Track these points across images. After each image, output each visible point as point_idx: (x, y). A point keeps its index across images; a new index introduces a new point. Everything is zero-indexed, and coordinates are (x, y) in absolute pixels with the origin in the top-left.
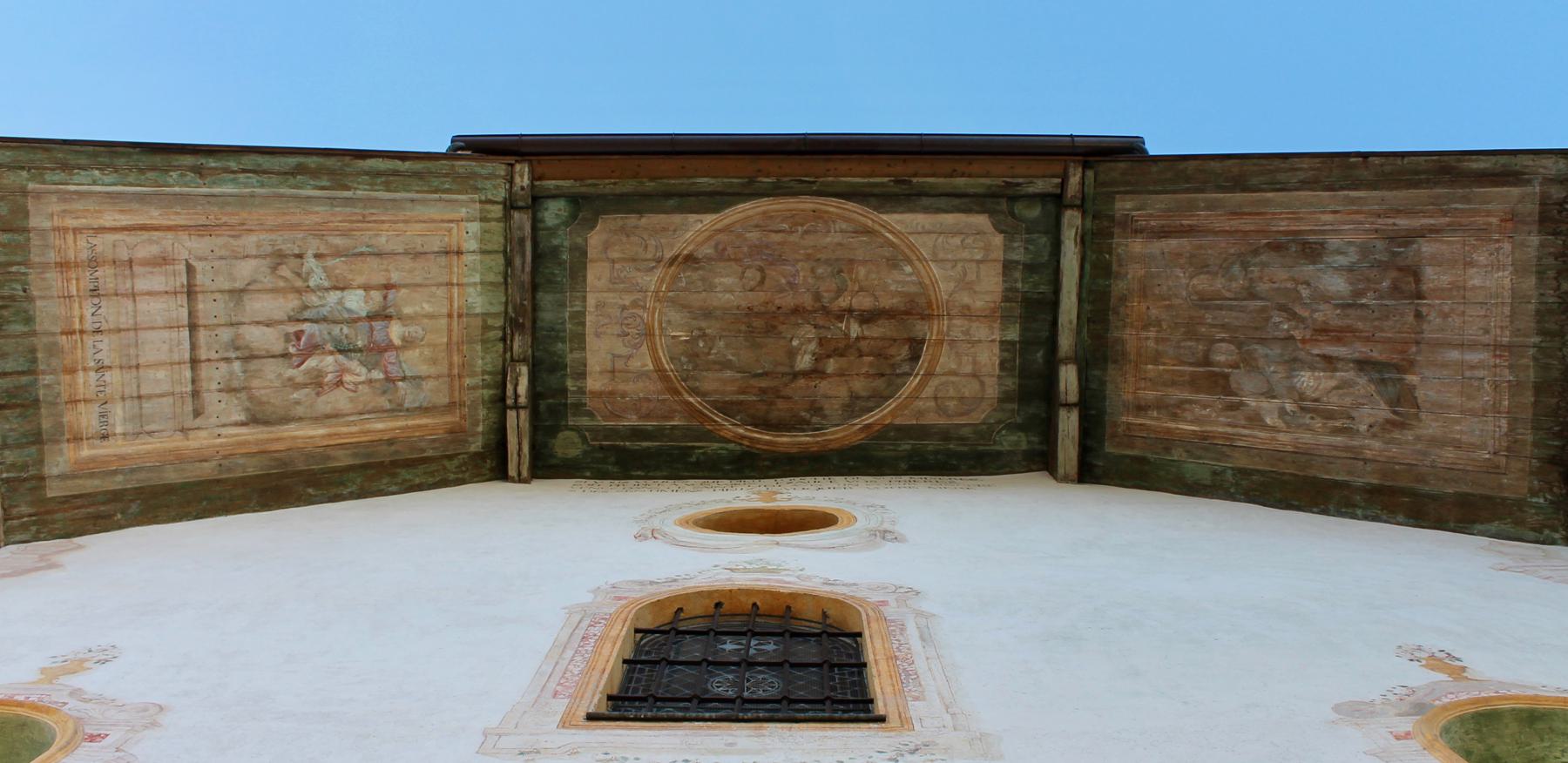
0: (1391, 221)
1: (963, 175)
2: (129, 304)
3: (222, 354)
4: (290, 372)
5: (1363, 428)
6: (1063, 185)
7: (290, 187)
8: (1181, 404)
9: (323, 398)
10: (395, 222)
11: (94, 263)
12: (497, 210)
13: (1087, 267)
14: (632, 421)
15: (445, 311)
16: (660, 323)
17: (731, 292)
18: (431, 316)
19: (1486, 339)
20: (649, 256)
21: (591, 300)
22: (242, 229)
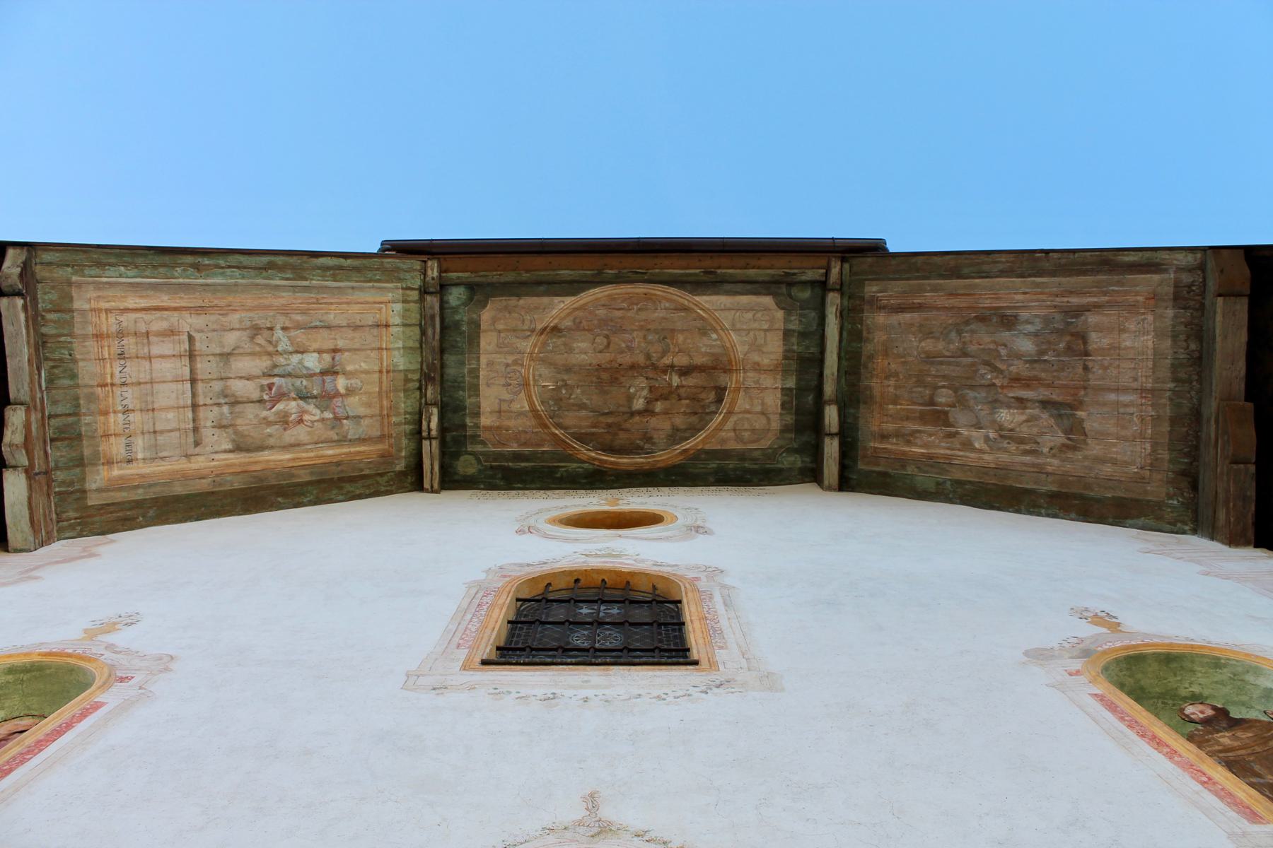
1: (753, 268)
4: (265, 413)
5: (1046, 450)
6: (827, 274)
8: (913, 433)
9: (288, 432)
11: (121, 334)
12: (414, 295)
13: (845, 334)
14: (514, 448)
15: (377, 368)
18: (367, 372)
19: (1135, 385)
21: (483, 360)
22: (229, 309)
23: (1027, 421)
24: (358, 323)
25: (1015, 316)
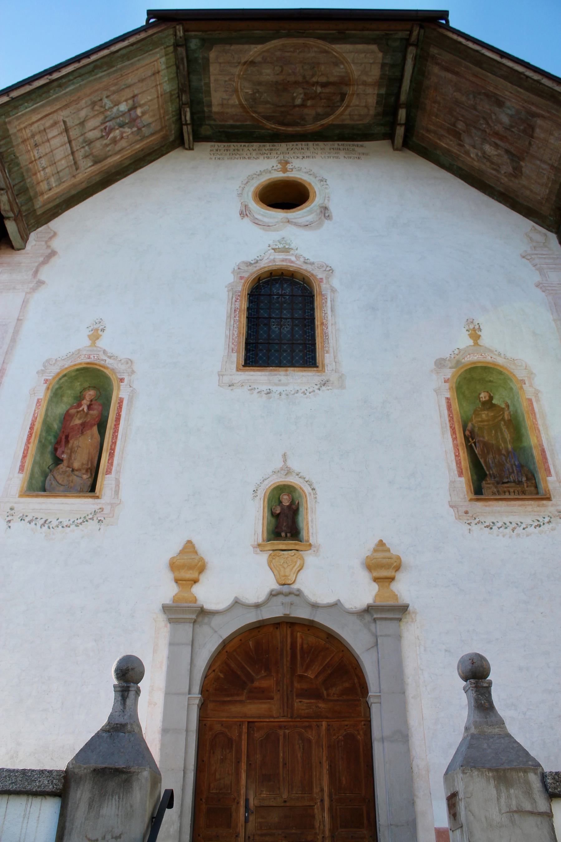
0: (529, 106)
1: (367, 30)
2: (48, 144)
3: (81, 146)
4: (105, 142)
5: (503, 172)
6: (410, 35)
7: (93, 76)
8: (442, 136)
9: (117, 145)
10: (133, 72)
11: (33, 136)
12: (171, 49)
13: (416, 69)
14: (231, 122)
15: (156, 96)
16: (241, 87)
17: (269, 75)
18: (151, 100)
19: (550, 162)
20: (235, 61)
21: (212, 78)
22: (79, 99)
23: (497, 155)
24: (144, 77)
25: (504, 103)
